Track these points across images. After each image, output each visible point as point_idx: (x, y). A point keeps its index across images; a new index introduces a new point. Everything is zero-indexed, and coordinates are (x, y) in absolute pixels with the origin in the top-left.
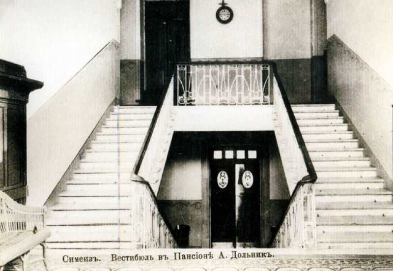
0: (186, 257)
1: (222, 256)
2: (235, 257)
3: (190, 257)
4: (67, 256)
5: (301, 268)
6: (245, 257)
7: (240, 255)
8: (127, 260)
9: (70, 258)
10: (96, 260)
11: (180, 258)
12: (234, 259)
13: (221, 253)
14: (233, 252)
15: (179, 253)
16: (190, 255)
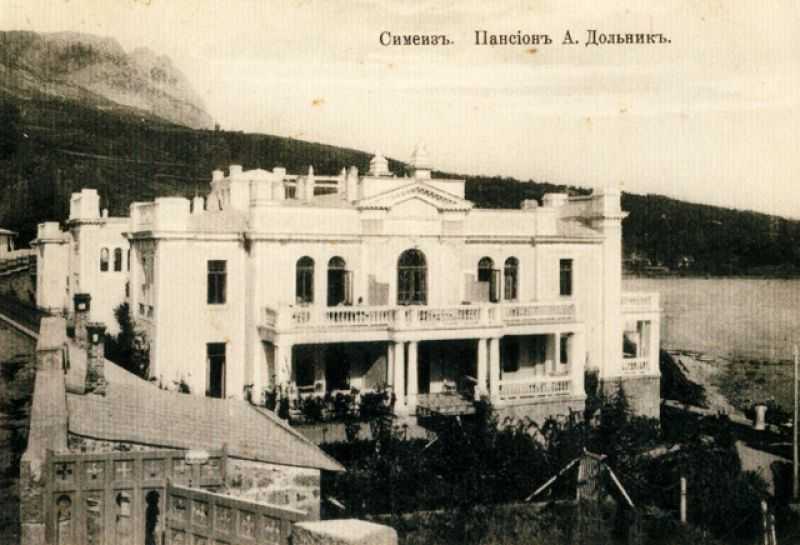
0: (498, 39)
2: (594, 42)
6: (613, 42)
7: (603, 38)
9: (395, 37)
11: (485, 42)
13: (568, 33)
14: (589, 31)
15: (485, 32)
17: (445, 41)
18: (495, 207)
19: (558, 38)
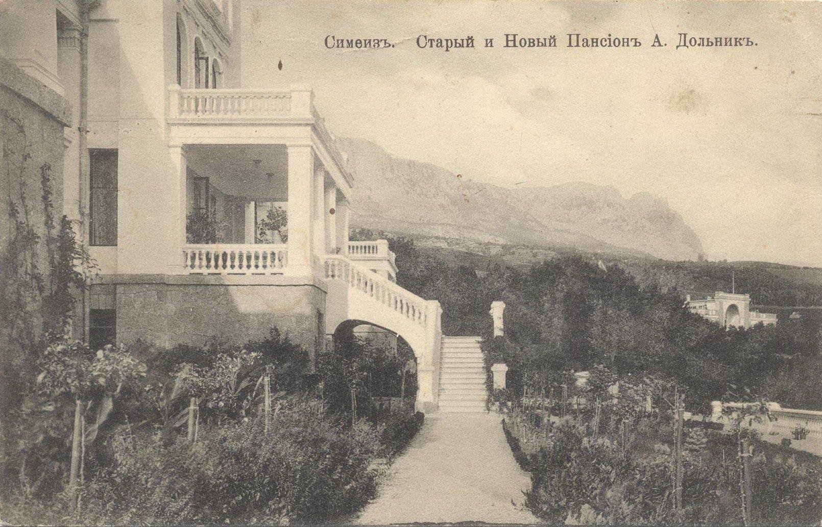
1: (659, 41)
2: (685, 45)
3: (597, 42)
4: (425, 37)
7: (693, 41)
8: (431, 46)
9: (338, 41)
12: (683, 49)
13: (657, 37)
14: (681, 34)
16: (529, 46)
17: (749, 43)
19: (647, 39)
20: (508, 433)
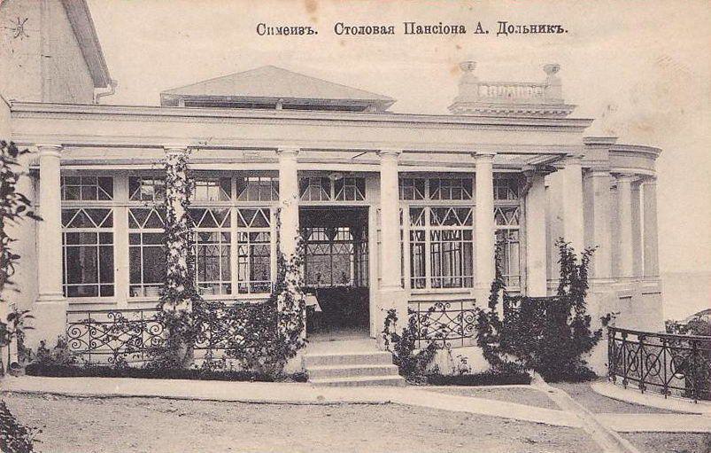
1: (481, 29)
2: (504, 32)
5: (623, 283)
10: (560, 30)
18: (368, 310)
20: (371, 104)
